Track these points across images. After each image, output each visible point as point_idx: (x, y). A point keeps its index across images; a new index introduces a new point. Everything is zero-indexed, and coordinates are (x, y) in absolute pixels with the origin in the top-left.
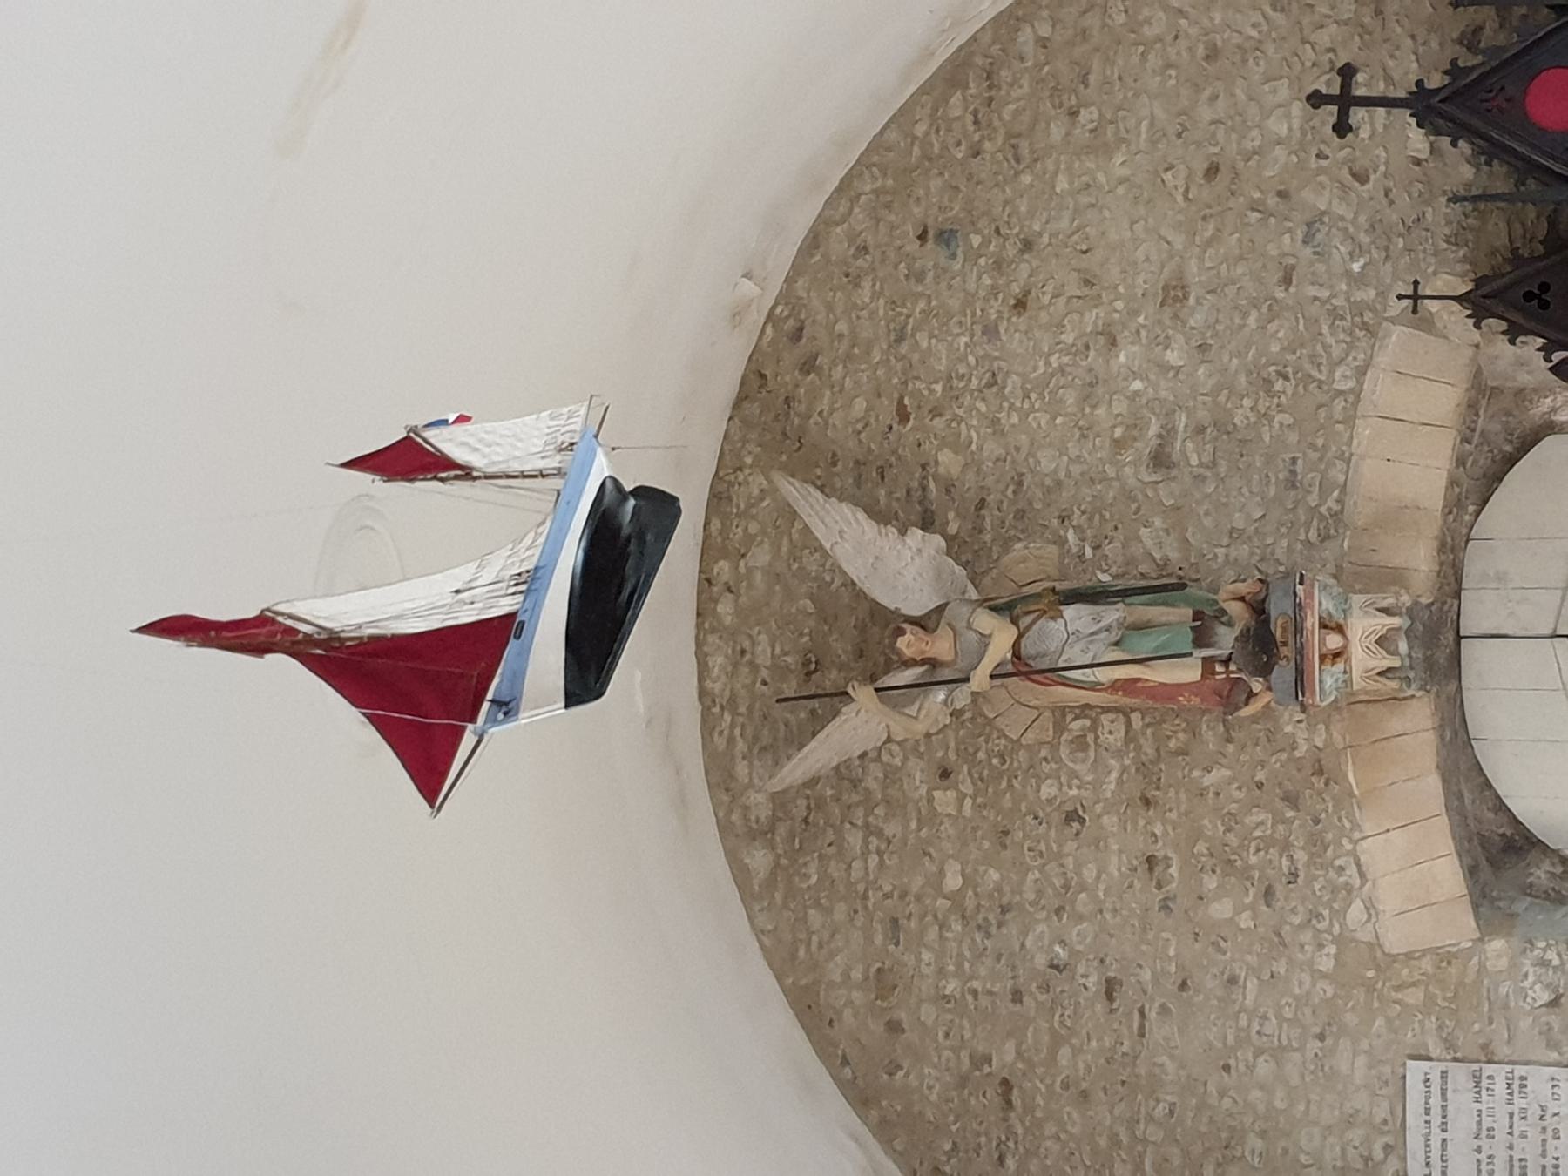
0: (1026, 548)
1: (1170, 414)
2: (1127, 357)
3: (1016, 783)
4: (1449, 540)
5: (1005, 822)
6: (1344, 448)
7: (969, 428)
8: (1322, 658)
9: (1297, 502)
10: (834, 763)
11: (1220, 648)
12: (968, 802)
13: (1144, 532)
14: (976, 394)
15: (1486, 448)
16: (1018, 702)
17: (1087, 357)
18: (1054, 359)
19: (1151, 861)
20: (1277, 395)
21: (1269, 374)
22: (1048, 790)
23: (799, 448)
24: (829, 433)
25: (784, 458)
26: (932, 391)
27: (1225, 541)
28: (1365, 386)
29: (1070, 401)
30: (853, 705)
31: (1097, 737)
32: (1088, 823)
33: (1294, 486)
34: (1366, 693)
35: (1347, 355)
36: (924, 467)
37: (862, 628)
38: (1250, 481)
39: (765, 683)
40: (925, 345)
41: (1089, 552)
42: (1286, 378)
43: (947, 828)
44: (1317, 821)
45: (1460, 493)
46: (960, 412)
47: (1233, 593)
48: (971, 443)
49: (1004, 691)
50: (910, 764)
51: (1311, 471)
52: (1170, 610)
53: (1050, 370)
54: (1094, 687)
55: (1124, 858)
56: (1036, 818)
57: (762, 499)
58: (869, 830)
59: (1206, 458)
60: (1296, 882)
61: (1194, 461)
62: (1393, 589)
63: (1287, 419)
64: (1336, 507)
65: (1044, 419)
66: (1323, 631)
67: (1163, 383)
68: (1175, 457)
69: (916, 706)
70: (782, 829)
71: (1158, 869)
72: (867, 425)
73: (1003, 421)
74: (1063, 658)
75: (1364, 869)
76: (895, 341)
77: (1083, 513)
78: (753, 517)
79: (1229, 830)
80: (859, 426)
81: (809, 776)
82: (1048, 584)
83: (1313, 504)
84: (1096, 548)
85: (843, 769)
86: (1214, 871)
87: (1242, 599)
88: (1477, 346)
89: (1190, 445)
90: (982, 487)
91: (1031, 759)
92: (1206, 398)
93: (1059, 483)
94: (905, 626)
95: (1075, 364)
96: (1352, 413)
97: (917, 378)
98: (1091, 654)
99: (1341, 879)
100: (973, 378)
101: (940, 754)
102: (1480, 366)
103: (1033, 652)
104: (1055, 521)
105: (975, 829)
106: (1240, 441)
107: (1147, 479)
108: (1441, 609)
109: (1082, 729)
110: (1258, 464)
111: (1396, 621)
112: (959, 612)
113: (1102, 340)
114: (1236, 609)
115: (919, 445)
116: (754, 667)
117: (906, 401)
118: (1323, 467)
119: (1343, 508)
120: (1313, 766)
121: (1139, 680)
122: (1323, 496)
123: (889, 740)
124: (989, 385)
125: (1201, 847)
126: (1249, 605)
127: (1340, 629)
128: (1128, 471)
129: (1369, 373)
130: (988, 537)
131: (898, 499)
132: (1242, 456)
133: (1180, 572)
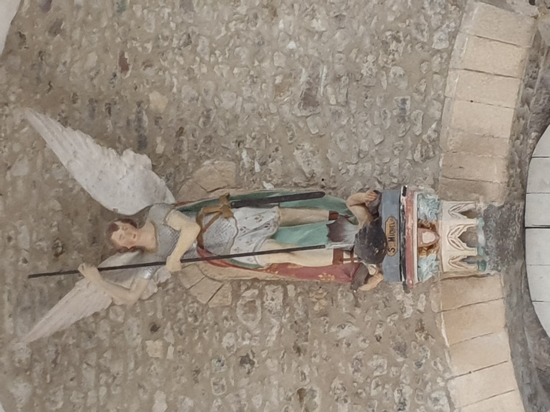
0: (213, 164)
1: (315, 67)
2: (284, 23)
3: (205, 336)
4: (517, 158)
5: (197, 364)
6: (440, 92)
7: (171, 75)
8: (420, 250)
9: (406, 132)
10: (73, 321)
11: (346, 242)
12: (171, 349)
13: (296, 153)
14: (176, 50)
15: (544, 91)
16: (206, 276)
17: (256, 24)
18: (232, 25)
19: (301, 393)
20: (393, 53)
21: (387, 37)
22: (228, 340)
23: (49, 90)
24: (71, 79)
25: (38, 96)
26: (145, 49)
27: (355, 160)
28: (455, 47)
29: (244, 56)
30: (84, 280)
31: (263, 303)
32: (256, 365)
33: (404, 121)
34: (455, 272)
35: (442, 23)
36: (139, 104)
37: (95, 221)
38: (372, 116)
39: (25, 261)
40: (139, 14)
41: (257, 168)
42: (398, 40)
43: (156, 367)
44: (419, 365)
45: (526, 124)
46: (166, 64)
47: (356, 201)
48: (173, 87)
49: (196, 268)
50: (130, 321)
51: (416, 109)
52: (314, 211)
53: (229, 34)
54: (257, 268)
55: (282, 390)
56: (220, 361)
57: (23, 127)
58: (100, 369)
59: (342, 99)
60: (404, 409)
61: (333, 101)
62: (475, 196)
63: (400, 71)
64: (434, 136)
65: (225, 69)
66: (421, 230)
67: (310, 44)
68: (319, 97)
69: (130, 281)
70: (38, 368)
71: (306, 400)
72: (98, 73)
73: (196, 72)
74: (234, 247)
75: (453, 400)
76: (118, 11)
77: (254, 138)
78: (17, 140)
79: (356, 371)
80: (92, 74)
81: (55, 329)
82: (226, 191)
83: (418, 133)
84: (263, 164)
85: (82, 325)
86: (346, 401)
87: (363, 205)
88: (536, 17)
89: (330, 90)
90: (181, 120)
91: (216, 318)
92: (341, 55)
93: (236, 117)
94: (118, 223)
95: (248, 30)
96: (445, 66)
97: (134, 39)
98: (253, 245)
99: (436, 408)
100: (174, 39)
101: (150, 314)
102: (538, 32)
103: (212, 243)
104: (233, 144)
105: (176, 369)
106: (366, 87)
107: (299, 115)
108: (509, 209)
109: (252, 296)
110: (378, 104)
111: (473, 222)
112: (157, 213)
113: (266, 12)
114: (359, 212)
115: (136, 88)
116: (17, 249)
117: (126, 56)
118: (425, 106)
119: (438, 137)
120: (417, 324)
121: (288, 264)
122: (425, 128)
123: (113, 304)
124: (186, 44)
125: (337, 383)
126: (367, 208)
127: (433, 228)
128: (286, 108)
129: (458, 37)
130: (185, 156)
131: (120, 128)
132: (366, 98)
133: (323, 183)
